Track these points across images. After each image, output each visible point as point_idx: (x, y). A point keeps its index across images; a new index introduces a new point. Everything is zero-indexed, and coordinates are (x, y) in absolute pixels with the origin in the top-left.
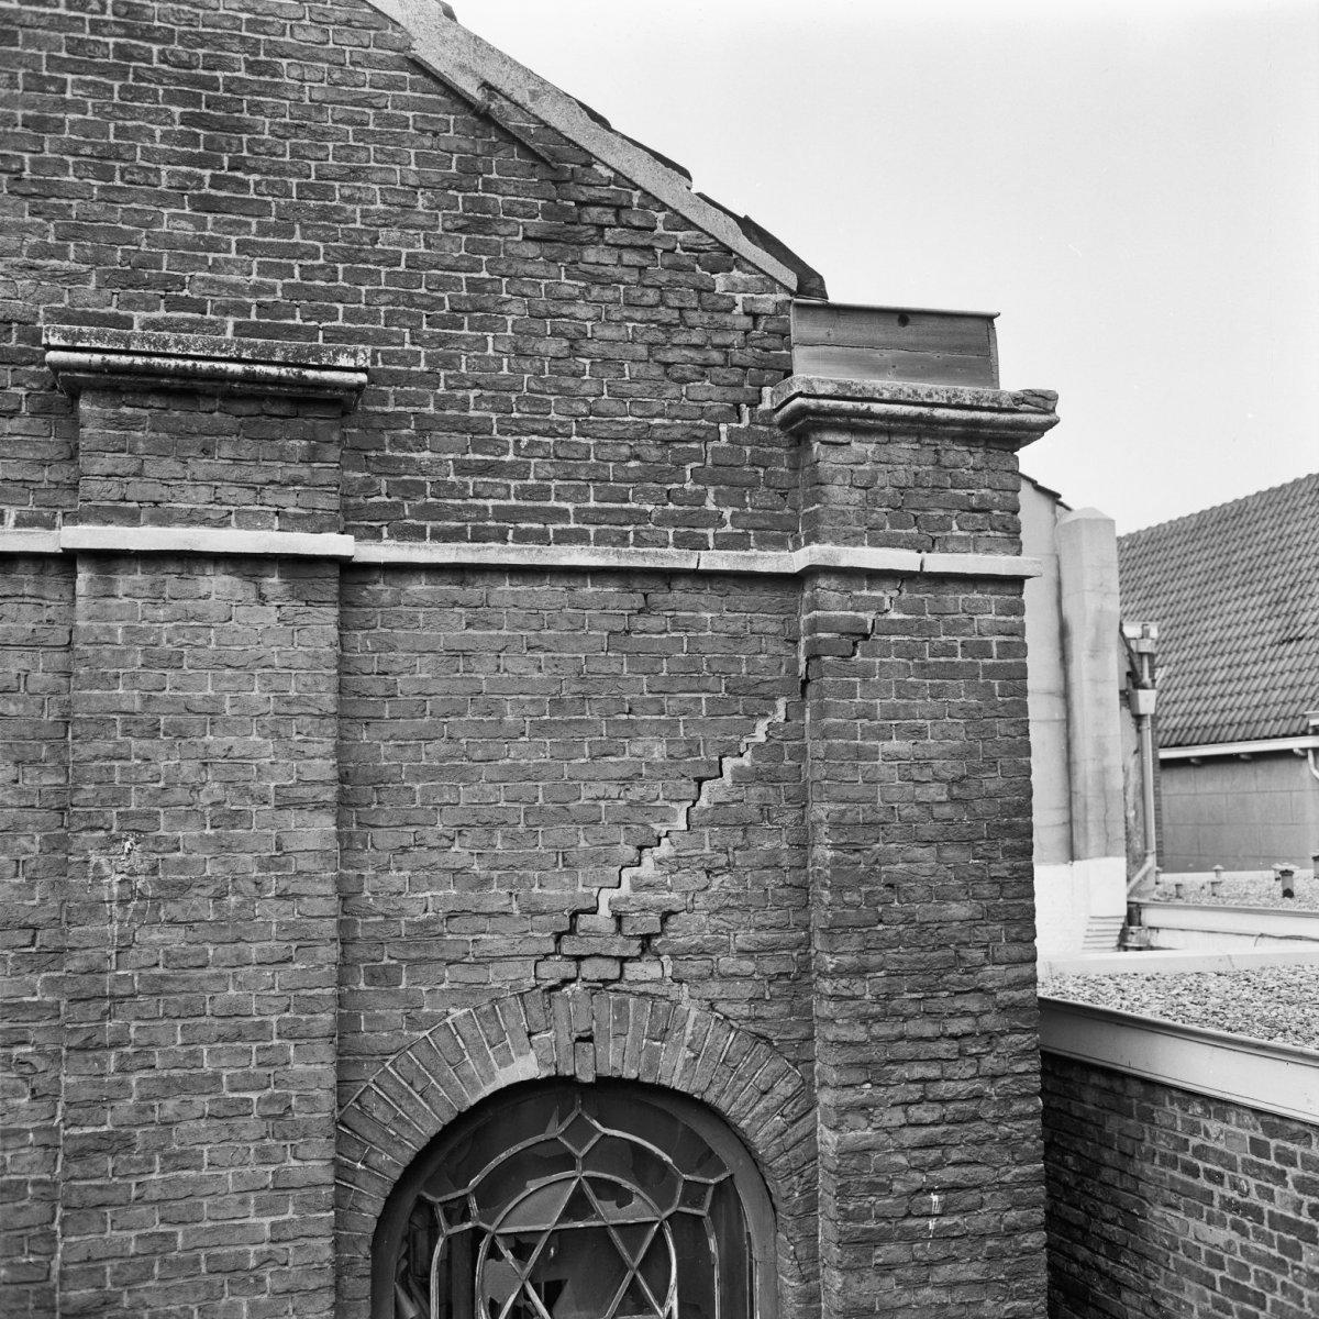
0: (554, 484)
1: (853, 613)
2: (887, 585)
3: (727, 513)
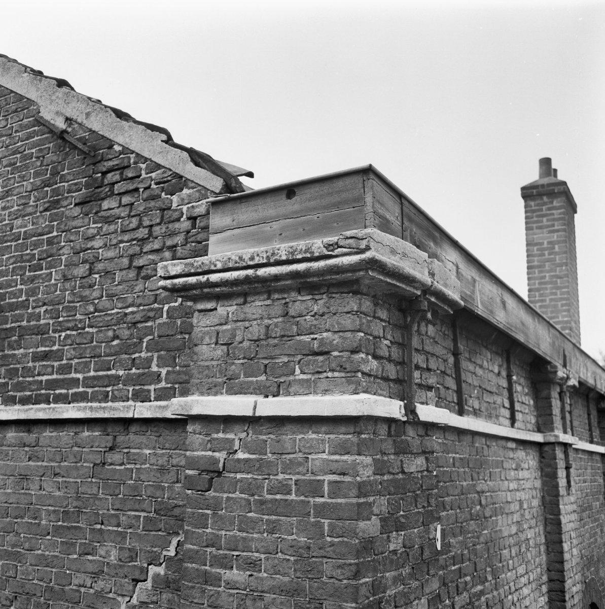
0: (74, 362)
1: (210, 453)
2: (237, 427)
3: (164, 371)
